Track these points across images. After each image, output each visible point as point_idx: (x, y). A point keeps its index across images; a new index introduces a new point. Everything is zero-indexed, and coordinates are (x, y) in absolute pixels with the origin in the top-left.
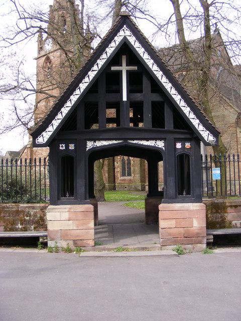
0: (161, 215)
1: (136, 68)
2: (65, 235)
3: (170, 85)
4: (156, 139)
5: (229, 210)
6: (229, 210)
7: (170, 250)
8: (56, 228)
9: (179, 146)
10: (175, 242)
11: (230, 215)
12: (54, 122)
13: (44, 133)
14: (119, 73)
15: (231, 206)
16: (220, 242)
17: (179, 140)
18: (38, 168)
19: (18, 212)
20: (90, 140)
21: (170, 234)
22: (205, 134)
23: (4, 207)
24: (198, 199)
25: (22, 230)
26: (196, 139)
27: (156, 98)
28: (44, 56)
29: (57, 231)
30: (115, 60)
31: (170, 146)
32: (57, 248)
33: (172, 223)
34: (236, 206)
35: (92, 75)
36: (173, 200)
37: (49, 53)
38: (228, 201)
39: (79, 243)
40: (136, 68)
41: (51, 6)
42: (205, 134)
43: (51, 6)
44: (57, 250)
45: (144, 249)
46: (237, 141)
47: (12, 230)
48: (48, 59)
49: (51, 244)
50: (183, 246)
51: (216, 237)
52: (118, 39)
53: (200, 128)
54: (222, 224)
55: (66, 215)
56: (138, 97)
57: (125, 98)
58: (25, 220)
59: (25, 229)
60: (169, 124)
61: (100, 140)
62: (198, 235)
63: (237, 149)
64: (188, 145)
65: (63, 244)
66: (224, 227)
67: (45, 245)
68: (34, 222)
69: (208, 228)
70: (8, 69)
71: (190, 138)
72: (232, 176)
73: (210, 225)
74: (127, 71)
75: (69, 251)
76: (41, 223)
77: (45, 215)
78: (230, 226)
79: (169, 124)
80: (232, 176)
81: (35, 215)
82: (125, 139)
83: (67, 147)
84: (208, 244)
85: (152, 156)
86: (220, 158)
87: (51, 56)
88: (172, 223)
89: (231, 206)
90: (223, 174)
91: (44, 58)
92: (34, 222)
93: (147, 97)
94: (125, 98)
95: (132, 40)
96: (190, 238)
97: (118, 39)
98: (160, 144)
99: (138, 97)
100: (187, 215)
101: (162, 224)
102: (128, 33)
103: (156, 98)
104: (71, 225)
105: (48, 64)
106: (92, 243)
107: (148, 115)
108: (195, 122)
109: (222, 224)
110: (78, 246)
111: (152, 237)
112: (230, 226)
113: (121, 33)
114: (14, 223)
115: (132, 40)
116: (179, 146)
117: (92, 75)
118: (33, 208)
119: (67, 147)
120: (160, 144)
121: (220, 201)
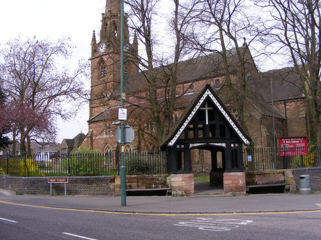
0: (224, 178)
1: (212, 108)
2: (180, 188)
3: (229, 118)
4: (222, 142)
5: (256, 176)
6: (256, 176)
7: (229, 194)
8: (176, 185)
9: (232, 145)
10: (231, 191)
11: (257, 179)
12: (176, 135)
13: (172, 141)
14: (204, 111)
15: (257, 175)
16: (254, 191)
17: (232, 143)
18: (144, 157)
19: (152, 179)
20: (191, 143)
21: (229, 187)
22: (245, 141)
23: (145, 177)
24: (242, 171)
25: (154, 188)
26: (240, 142)
27: (221, 123)
28: (98, 57)
29: (177, 187)
30: (203, 105)
31: (228, 145)
32: (177, 194)
33: (230, 182)
34: (259, 174)
35: (193, 113)
36: (230, 171)
37: (103, 55)
38: (255, 172)
39: (187, 191)
40: (212, 108)
41: (103, 14)
42: (245, 141)
43: (103, 14)
44: (177, 195)
45: (217, 194)
46: (261, 134)
47: (149, 188)
48: (102, 61)
49: (173, 193)
50: (235, 193)
51: (250, 188)
52: (205, 96)
53: (243, 138)
54: (253, 183)
55: (181, 179)
56: (213, 122)
57: (207, 123)
58: (156, 183)
59: (156, 187)
60: (228, 136)
61: (195, 143)
62: (242, 187)
63: (261, 140)
64: (236, 145)
65: (180, 193)
66: (254, 185)
67: (170, 194)
68: (161, 184)
69: (246, 185)
70: (84, 76)
71: (95, 43)
72: (258, 159)
73: (248, 183)
74: (208, 110)
75: (182, 195)
76: (164, 184)
77: (166, 180)
78: (257, 184)
79: (228, 136)
80: (258, 159)
81: (161, 180)
82: (208, 143)
83: (180, 146)
84: (247, 192)
85: (214, 150)
86: (250, 151)
87: (105, 58)
88: (230, 182)
89: (257, 175)
90: (253, 157)
91: (97, 60)
92: (161, 184)
93: (217, 122)
94: (207, 123)
95: (211, 96)
96: (238, 189)
97: (205, 96)
98: (224, 145)
99: (213, 122)
100: (237, 178)
101: (225, 182)
102: (209, 93)
103: (221, 123)
104: (183, 184)
105: (101, 64)
106: (193, 192)
107: (218, 131)
108: (241, 135)
109: (253, 183)
110: (187, 193)
111: (219, 191)
112: (257, 184)
113: (206, 93)
114: (151, 184)
115: (211, 96)
116: (232, 145)
117: (193, 113)
118: (161, 176)
119: (180, 146)
120: (224, 145)
121: (252, 172)
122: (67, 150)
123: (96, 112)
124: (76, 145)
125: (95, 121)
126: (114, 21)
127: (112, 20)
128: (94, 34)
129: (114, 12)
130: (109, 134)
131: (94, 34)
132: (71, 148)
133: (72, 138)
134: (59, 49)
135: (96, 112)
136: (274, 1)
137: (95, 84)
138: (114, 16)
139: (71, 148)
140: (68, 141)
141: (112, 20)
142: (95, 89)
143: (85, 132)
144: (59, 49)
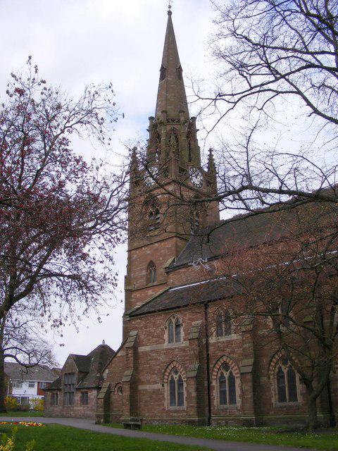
41: (151, 118)
43: (151, 118)
83: (295, 359)
119: (295, 359)
122: (76, 376)
123: (138, 300)
124: (94, 367)
125: (143, 314)
126: (174, 130)
127: (168, 128)
128: (171, 71)
129: (172, 114)
130: (178, 340)
131: (171, 71)
132: (84, 373)
133: (85, 352)
134: (88, 115)
135: (138, 300)
136: (301, 2)
137: (136, 245)
138: (173, 120)
139: (84, 373)
140: (76, 360)
141: (168, 128)
142: (136, 254)
143: (115, 343)
144: (88, 115)
